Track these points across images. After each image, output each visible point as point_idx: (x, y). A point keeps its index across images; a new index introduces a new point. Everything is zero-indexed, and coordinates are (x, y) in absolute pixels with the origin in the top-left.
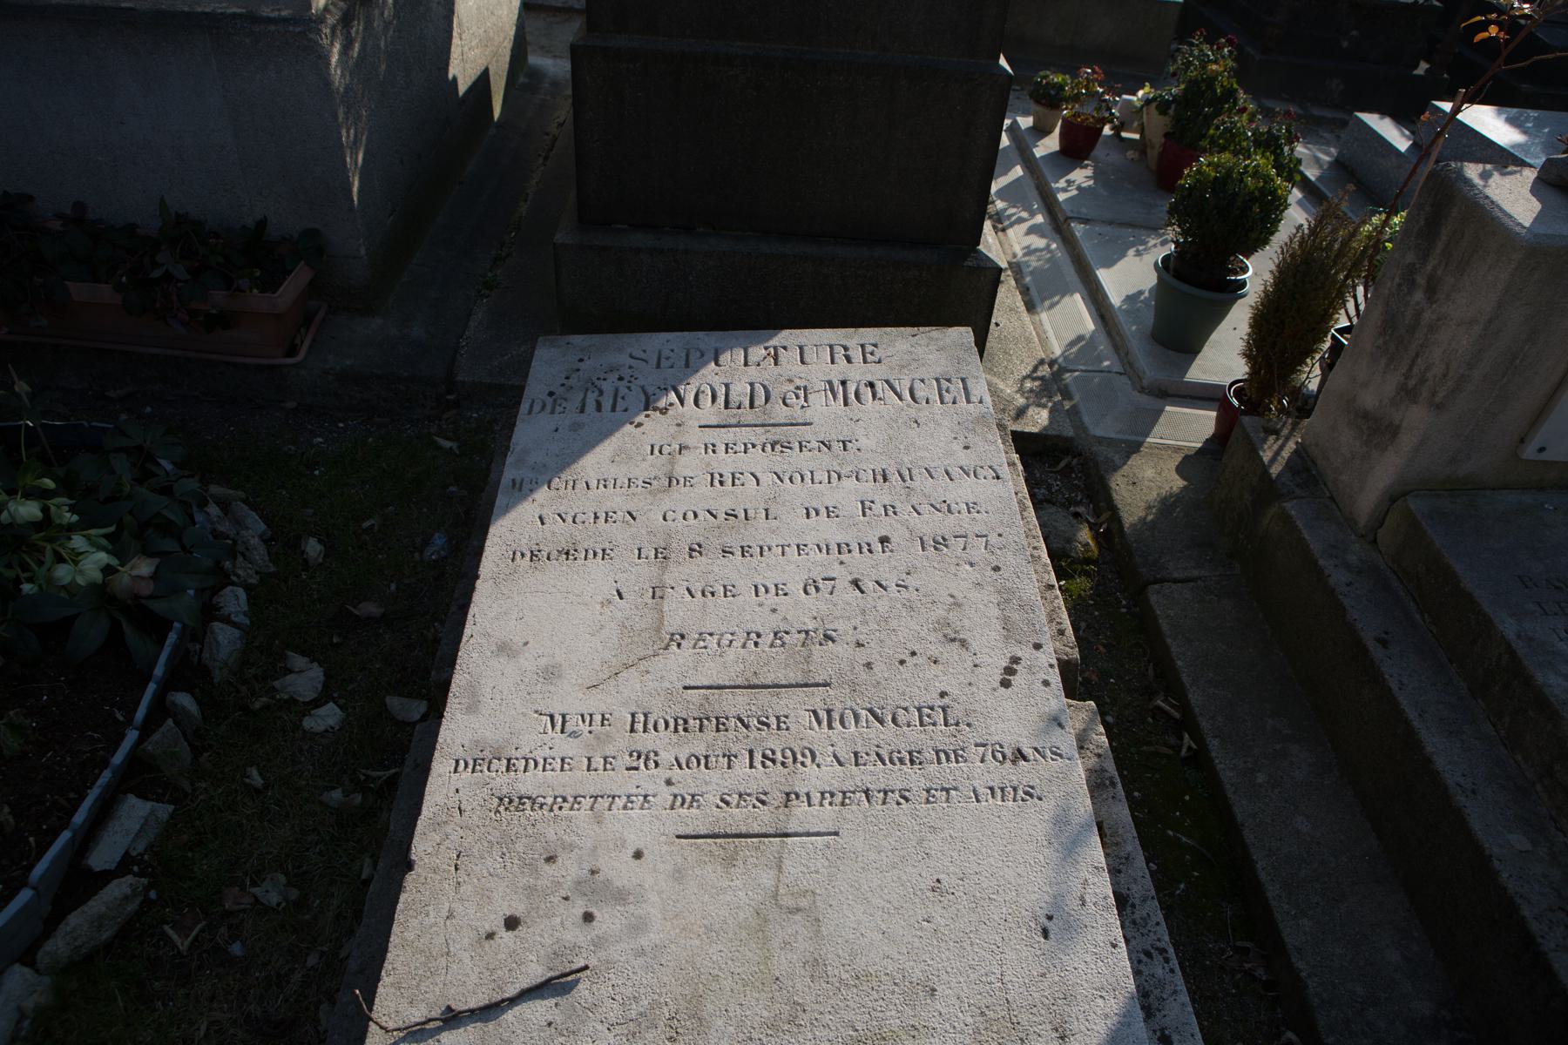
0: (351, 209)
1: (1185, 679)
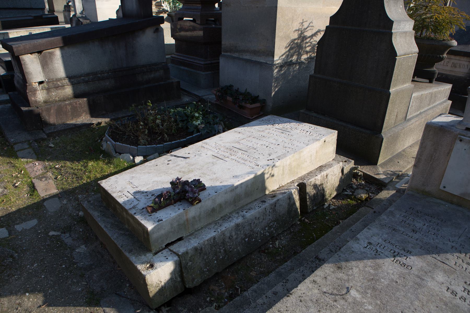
0: (271, 97)
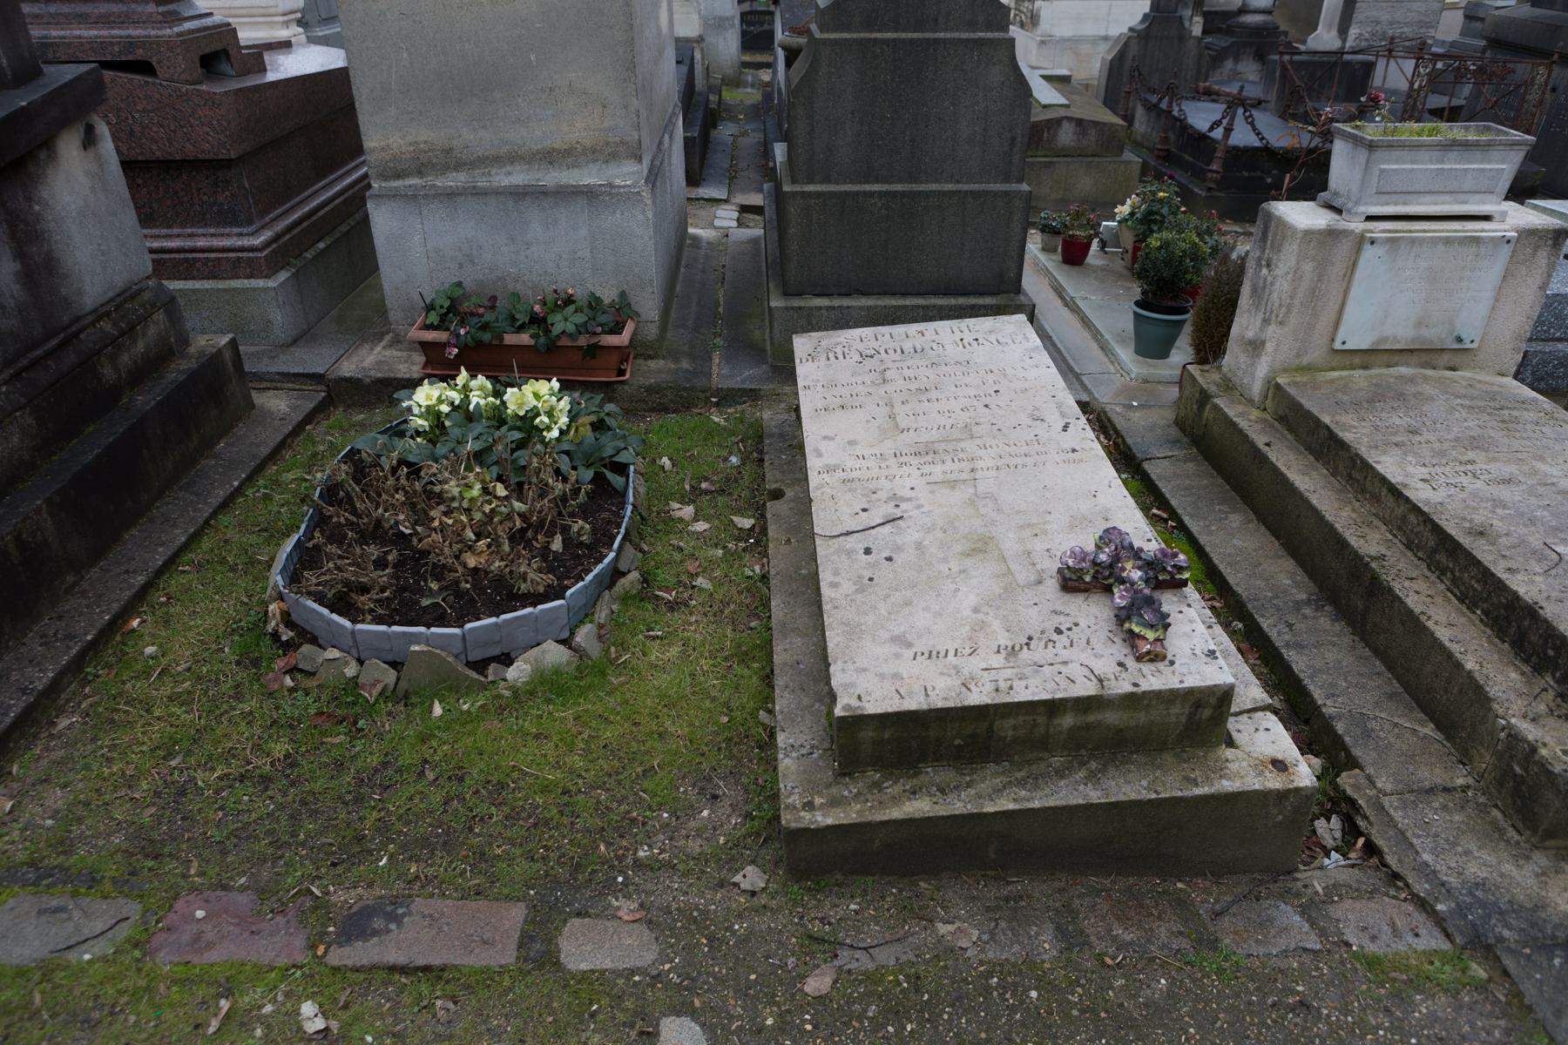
1: (1167, 496)
